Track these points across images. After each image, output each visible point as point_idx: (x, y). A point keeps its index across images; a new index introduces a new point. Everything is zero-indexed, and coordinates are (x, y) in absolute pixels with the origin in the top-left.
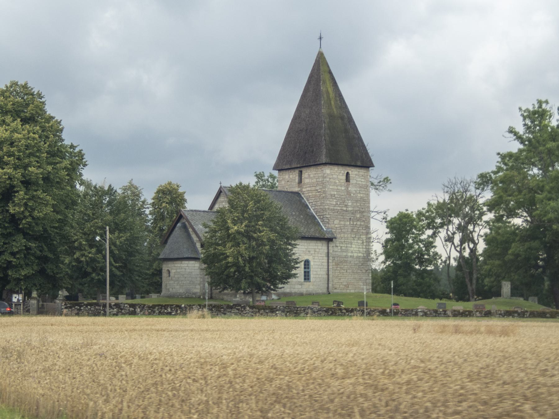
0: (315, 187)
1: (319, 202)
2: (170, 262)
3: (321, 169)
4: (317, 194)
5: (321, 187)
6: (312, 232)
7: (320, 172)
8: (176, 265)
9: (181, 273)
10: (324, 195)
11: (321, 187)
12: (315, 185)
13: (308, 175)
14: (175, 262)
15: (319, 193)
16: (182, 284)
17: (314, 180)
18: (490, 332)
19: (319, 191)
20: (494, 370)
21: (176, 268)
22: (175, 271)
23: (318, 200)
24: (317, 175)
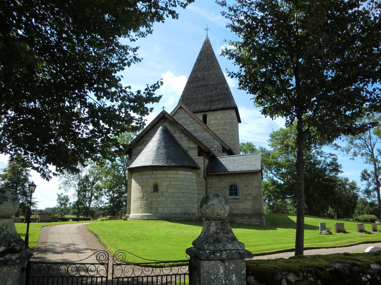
0: (223, 126)
1: (228, 138)
2: (159, 172)
3: (229, 112)
4: (226, 132)
5: (230, 126)
6: (187, 164)
7: (227, 115)
8: (169, 176)
9: (177, 186)
10: (233, 133)
11: (230, 126)
12: (223, 125)
13: (215, 117)
14: (167, 172)
15: (228, 132)
16: (178, 202)
17: (222, 121)
18: (328, 245)
19: (228, 129)
20: (150, 193)
21: (168, 180)
22: (168, 183)
23: (226, 137)
24: (224, 117)
